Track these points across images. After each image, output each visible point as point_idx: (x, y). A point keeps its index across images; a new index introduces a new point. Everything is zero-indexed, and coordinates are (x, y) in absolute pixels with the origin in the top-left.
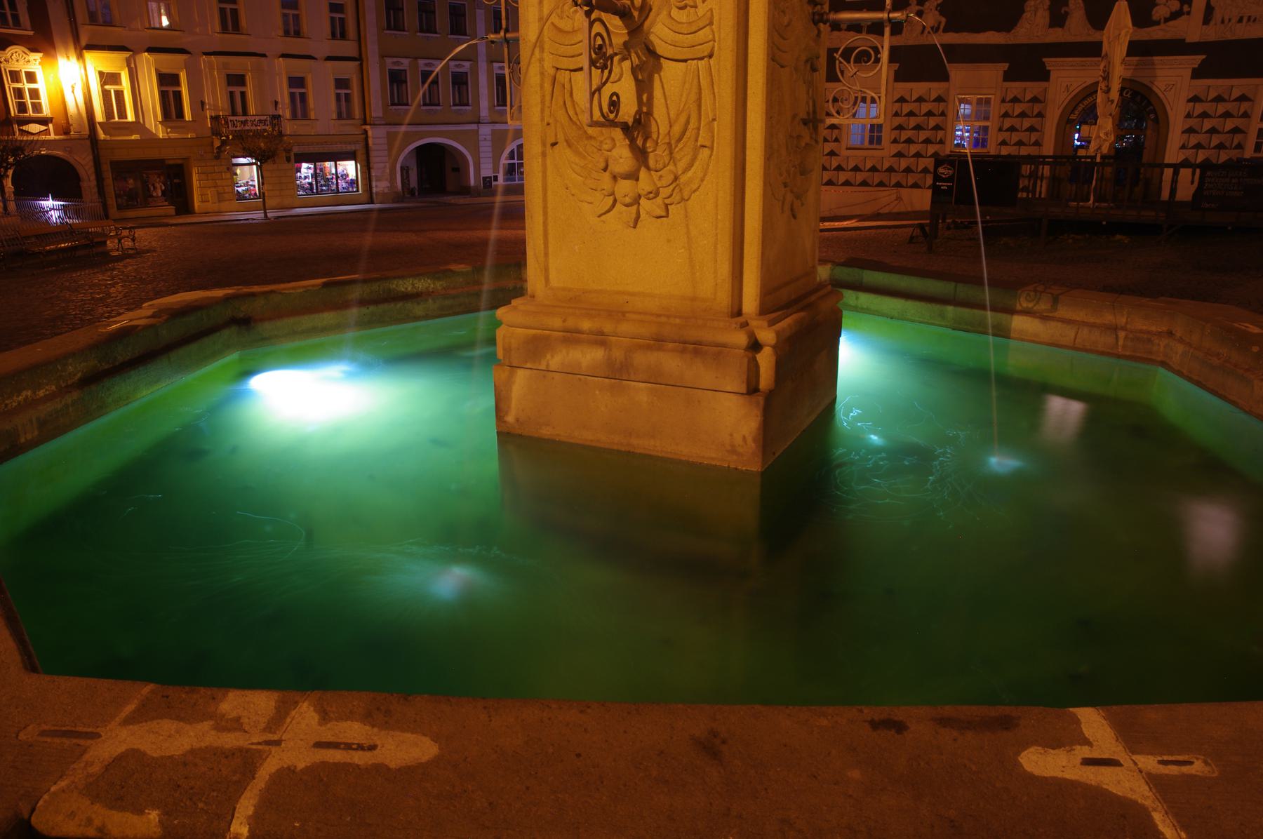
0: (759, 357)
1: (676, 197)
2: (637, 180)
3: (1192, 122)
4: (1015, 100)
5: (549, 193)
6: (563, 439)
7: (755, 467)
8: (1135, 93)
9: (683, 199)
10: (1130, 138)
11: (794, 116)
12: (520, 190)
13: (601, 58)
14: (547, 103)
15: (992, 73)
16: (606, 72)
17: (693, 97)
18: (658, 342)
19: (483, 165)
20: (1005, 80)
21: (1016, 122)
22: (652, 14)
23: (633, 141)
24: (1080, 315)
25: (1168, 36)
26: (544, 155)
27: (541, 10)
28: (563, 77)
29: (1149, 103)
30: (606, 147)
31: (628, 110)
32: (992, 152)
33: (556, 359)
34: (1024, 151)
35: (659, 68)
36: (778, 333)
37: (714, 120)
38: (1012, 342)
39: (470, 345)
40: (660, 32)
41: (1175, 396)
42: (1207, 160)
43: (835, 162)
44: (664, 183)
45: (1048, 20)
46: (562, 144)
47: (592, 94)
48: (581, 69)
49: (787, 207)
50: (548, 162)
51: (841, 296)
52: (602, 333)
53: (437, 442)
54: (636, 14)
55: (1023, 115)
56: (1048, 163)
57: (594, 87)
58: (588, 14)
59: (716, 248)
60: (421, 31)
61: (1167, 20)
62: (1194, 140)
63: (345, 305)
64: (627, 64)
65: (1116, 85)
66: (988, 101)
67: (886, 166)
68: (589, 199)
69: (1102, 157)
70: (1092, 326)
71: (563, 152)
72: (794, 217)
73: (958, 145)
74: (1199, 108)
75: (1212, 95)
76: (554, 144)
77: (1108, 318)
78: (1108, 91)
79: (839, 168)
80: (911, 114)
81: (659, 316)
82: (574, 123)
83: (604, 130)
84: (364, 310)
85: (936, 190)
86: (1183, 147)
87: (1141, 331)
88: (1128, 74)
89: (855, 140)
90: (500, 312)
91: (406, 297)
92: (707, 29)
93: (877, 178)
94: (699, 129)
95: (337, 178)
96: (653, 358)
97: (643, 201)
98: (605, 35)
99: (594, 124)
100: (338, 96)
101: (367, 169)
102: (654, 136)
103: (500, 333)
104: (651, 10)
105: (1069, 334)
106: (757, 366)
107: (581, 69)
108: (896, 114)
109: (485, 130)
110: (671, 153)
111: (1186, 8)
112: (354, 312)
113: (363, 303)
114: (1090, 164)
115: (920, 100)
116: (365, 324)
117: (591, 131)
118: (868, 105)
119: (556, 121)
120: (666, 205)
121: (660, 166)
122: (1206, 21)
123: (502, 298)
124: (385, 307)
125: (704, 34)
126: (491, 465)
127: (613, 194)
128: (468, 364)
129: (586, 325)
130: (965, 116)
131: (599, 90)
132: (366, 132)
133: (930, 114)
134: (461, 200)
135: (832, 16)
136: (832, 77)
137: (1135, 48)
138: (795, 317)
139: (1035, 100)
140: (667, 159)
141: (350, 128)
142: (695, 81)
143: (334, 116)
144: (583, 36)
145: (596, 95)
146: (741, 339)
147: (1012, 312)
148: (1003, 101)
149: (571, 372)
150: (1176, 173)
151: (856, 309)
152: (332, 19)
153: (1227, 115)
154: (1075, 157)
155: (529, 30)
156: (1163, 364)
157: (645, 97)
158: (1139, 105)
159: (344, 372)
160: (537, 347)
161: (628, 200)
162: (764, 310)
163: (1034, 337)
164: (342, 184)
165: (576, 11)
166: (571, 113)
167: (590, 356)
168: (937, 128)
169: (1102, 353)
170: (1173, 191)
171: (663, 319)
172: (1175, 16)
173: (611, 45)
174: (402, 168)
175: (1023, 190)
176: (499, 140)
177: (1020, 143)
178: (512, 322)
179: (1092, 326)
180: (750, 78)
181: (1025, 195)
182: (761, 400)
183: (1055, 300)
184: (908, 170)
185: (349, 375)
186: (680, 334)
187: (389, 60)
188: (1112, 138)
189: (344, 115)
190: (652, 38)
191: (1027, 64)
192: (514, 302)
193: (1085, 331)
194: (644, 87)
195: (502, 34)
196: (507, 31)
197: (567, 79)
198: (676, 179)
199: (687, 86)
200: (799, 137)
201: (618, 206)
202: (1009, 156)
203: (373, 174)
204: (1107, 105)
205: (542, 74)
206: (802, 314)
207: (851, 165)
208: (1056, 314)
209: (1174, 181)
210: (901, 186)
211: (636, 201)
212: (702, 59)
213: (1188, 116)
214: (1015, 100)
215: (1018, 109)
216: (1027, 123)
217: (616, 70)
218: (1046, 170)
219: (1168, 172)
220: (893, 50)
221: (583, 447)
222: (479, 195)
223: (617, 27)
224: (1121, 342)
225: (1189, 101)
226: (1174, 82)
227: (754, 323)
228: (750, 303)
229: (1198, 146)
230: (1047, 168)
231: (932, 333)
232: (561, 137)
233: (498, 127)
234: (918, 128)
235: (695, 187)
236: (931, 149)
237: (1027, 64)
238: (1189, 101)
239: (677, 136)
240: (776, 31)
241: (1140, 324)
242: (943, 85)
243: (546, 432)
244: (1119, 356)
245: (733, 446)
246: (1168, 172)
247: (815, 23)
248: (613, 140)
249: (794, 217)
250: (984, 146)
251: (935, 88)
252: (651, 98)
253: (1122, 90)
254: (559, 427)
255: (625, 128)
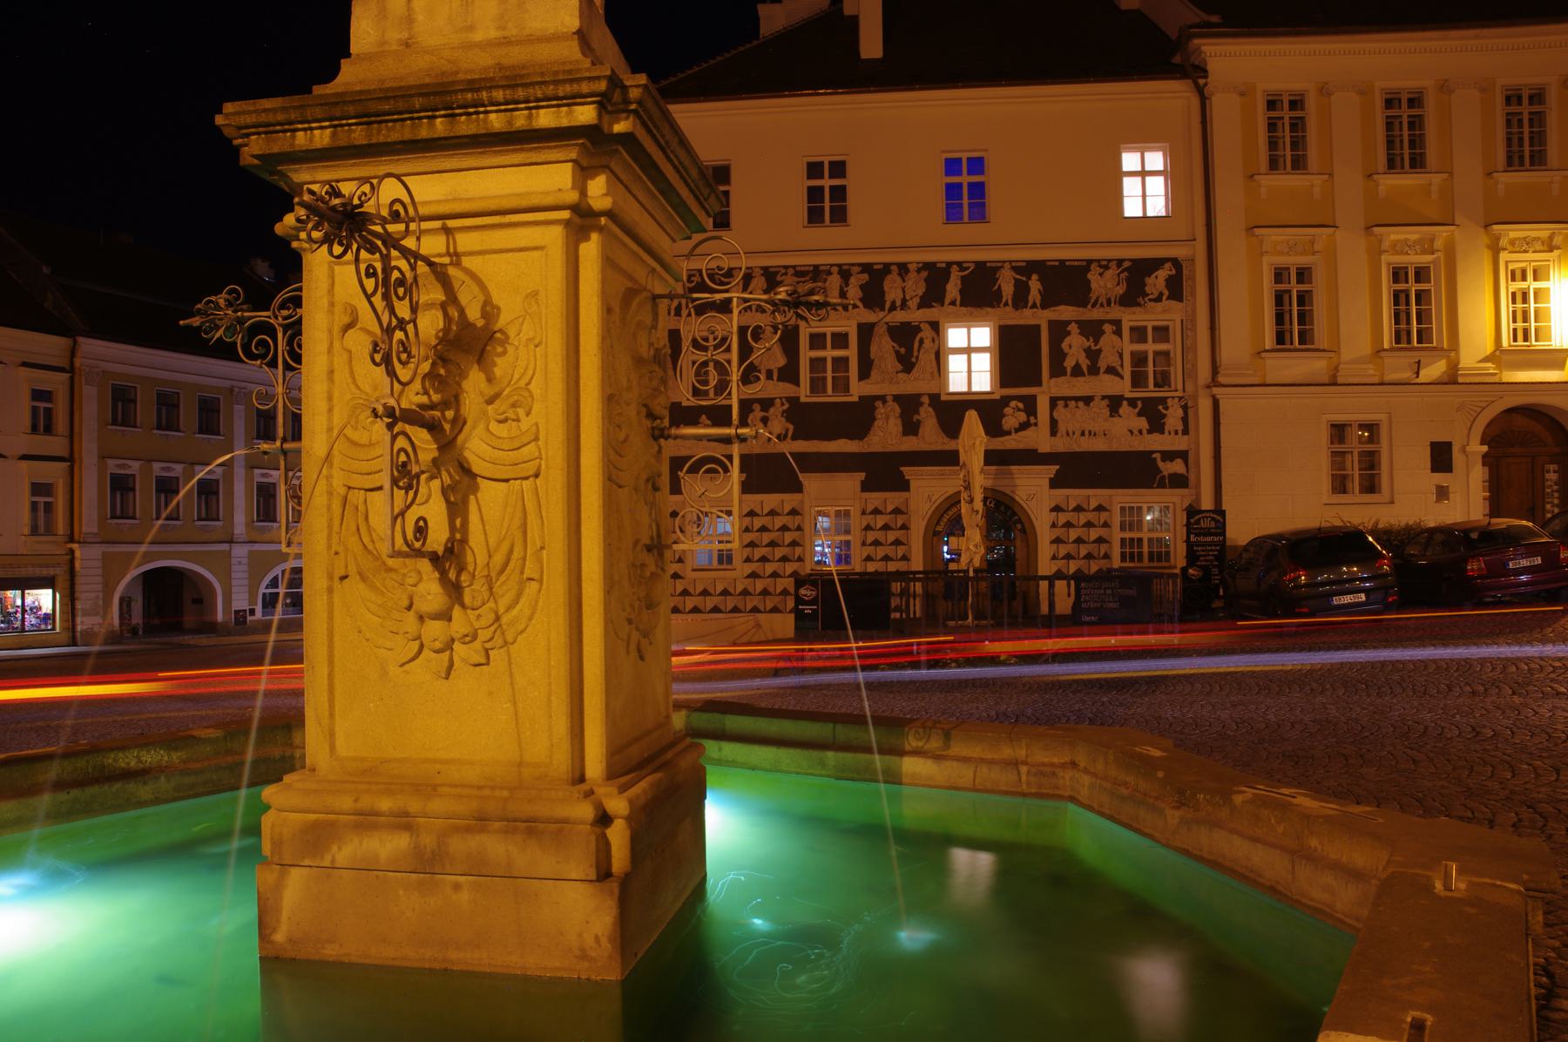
0: (609, 832)
1: (498, 641)
2: (450, 620)
3: (1058, 532)
4: (876, 512)
5: (337, 638)
6: (354, 959)
7: (614, 974)
8: (998, 503)
9: (506, 643)
10: (999, 552)
11: (636, 543)
12: (298, 626)
13: (405, 476)
14: (336, 528)
15: (849, 483)
16: (411, 493)
17: (517, 522)
18: (481, 822)
19: (234, 594)
20: (863, 490)
21: (879, 535)
22: (467, 428)
23: (443, 574)
24: (976, 751)
25: (1021, 446)
26: (330, 590)
27: (330, 420)
28: (357, 497)
29: (1014, 514)
30: (410, 581)
31: (438, 537)
32: (858, 570)
33: (345, 852)
34: (892, 567)
35: (474, 489)
36: (631, 802)
37: (542, 548)
38: (906, 790)
39: (225, 835)
40: (476, 447)
41: (1091, 835)
42: (1079, 571)
43: (680, 586)
44: (483, 622)
45: (900, 429)
46: (354, 578)
47: (395, 519)
48: (380, 488)
49: (633, 647)
50: (336, 599)
51: (701, 749)
52: (406, 814)
53: (166, 980)
54: (447, 427)
55: (886, 527)
56: (919, 580)
57: (397, 511)
58: (390, 427)
59: (549, 700)
60: (158, 428)
61: (1017, 431)
62: (1063, 550)
63: (34, 790)
64: (436, 484)
65: (979, 497)
66: (847, 513)
67: (740, 588)
68: (388, 645)
69: (976, 571)
70: (991, 762)
71: (355, 586)
72: (642, 658)
73: (819, 562)
74: (1062, 518)
75: (1072, 505)
76: (343, 578)
77: (1007, 752)
78: (971, 501)
79: (685, 593)
80: (763, 529)
81: (480, 788)
82: (370, 552)
83: (407, 561)
84: (62, 796)
85: (800, 616)
86: (1054, 558)
87: (1044, 764)
88: (989, 483)
89: (702, 561)
90: (269, 792)
91: (128, 775)
92: (532, 446)
93: (731, 602)
94: (524, 559)
95: (24, 611)
96: (474, 842)
97: (456, 646)
98: (410, 450)
99: (396, 554)
100: (34, 506)
101: (70, 600)
102: (471, 568)
103: (267, 821)
104: (465, 423)
105: (965, 773)
106: (608, 844)
107: (380, 488)
108: (747, 530)
109: (240, 552)
110: (491, 589)
111: (1032, 420)
112: (46, 800)
113: (59, 786)
114: (963, 578)
115: (772, 513)
116: (58, 815)
117: (391, 562)
118: (717, 521)
119: (347, 549)
120: (487, 651)
121: (477, 603)
122: (1054, 432)
123: (274, 769)
124: (94, 790)
125: (529, 451)
126: (251, 1004)
127: (419, 638)
128: (218, 864)
129: (385, 804)
130: (825, 530)
131: (402, 514)
132: (72, 552)
133: (784, 528)
134: (203, 640)
135: (673, 431)
136: (676, 489)
137: (992, 458)
138: (649, 779)
139: (897, 511)
140: (486, 595)
141: (44, 545)
142: (520, 504)
143: (27, 531)
144: (384, 449)
145: (399, 520)
146: (586, 811)
147: (902, 753)
148: (864, 513)
149: (365, 867)
150: (1051, 586)
151: (720, 762)
152: (35, 410)
153: (1089, 525)
154: (946, 571)
155: (315, 441)
156: (1072, 799)
157: (458, 522)
158: (1004, 516)
159: (17, 887)
160: (317, 837)
161: (438, 645)
162: (612, 774)
163: (926, 782)
164: (31, 620)
165: (373, 423)
166: (366, 540)
167: (389, 846)
168: (794, 544)
169: (1006, 793)
170: (1052, 605)
171: (486, 792)
172: (1024, 426)
173: (417, 462)
174: (122, 600)
175: (895, 610)
176: (259, 564)
177: (886, 558)
178: (285, 805)
179: (991, 762)
180: (583, 500)
181: (898, 615)
182: (615, 887)
183: (947, 736)
184: (765, 592)
185: (29, 891)
186: (510, 811)
187: (110, 462)
188: (982, 550)
189: (42, 530)
190: (467, 454)
191: (884, 473)
192: (287, 779)
193: (984, 770)
194: (457, 509)
195: (278, 443)
196: (284, 440)
197: (361, 500)
198: (498, 618)
199: (509, 509)
200: (643, 565)
201: (426, 652)
202: (876, 573)
203: (79, 606)
204: (973, 514)
205: (330, 493)
206: (659, 775)
207: (700, 589)
208: (951, 752)
209: (1051, 594)
210: (759, 611)
211: (449, 645)
212: (526, 478)
213: (1054, 525)
214: (876, 512)
215: (880, 521)
216: (891, 536)
217: (423, 490)
218: (919, 587)
219: (1044, 585)
220: (743, 457)
221: (379, 968)
222: (229, 633)
223: (423, 441)
224: (1024, 778)
225: (1052, 510)
226: (1033, 490)
227: (601, 791)
228: (595, 766)
229: (1068, 557)
230: (919, 585)
231: (809, 783)
232: (352, 570)
233: (257, 547)
234: (772, 544)
235: (521, 627)
236: (790, 568)
237: (884, 473)
238: (1052, 510)
239: (498, 568)
240: (613, 449)
241: (1041, 756)
242: (797, 496)
243: (330, 952)
244: (1024, 795)
245: (582, 950)
246: (1044, 585)
247: (655, 438)
248: (419, 573)
249: (642, 658)
250: (848, 563)
251: (788, 500)
252: (465, 523)
253: (985, 499)
254: (350, 943)
255: (435, 559)
